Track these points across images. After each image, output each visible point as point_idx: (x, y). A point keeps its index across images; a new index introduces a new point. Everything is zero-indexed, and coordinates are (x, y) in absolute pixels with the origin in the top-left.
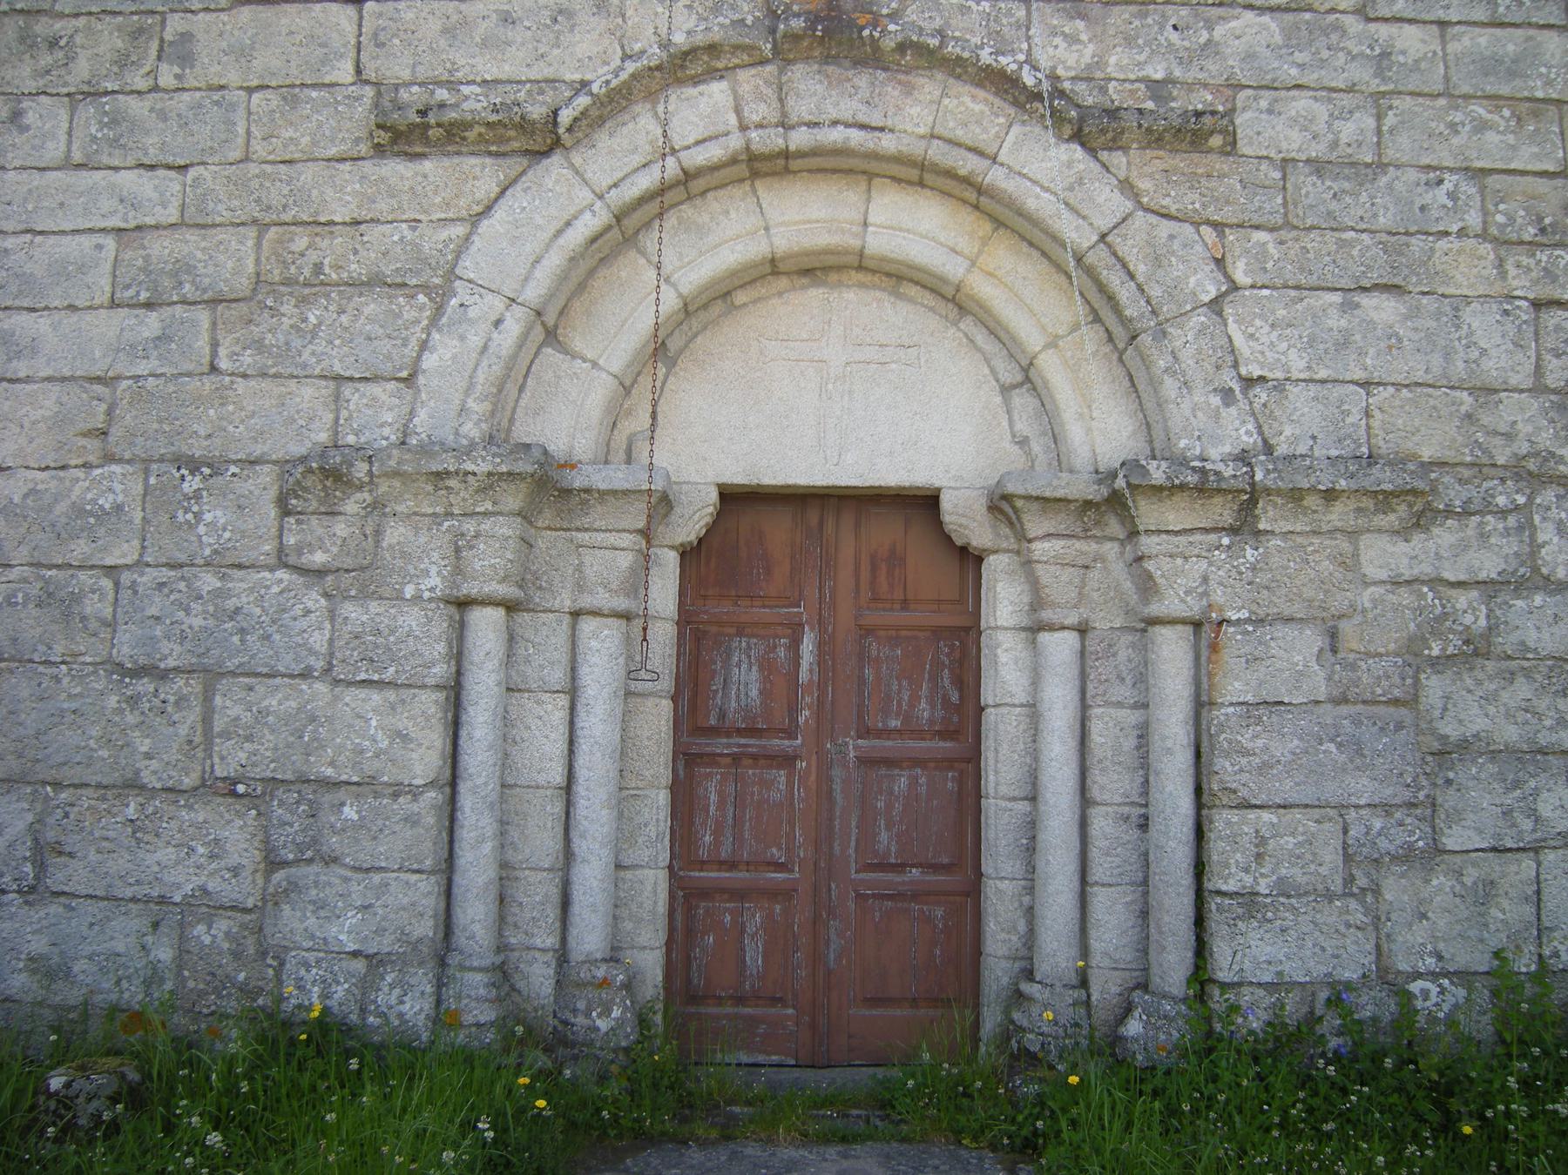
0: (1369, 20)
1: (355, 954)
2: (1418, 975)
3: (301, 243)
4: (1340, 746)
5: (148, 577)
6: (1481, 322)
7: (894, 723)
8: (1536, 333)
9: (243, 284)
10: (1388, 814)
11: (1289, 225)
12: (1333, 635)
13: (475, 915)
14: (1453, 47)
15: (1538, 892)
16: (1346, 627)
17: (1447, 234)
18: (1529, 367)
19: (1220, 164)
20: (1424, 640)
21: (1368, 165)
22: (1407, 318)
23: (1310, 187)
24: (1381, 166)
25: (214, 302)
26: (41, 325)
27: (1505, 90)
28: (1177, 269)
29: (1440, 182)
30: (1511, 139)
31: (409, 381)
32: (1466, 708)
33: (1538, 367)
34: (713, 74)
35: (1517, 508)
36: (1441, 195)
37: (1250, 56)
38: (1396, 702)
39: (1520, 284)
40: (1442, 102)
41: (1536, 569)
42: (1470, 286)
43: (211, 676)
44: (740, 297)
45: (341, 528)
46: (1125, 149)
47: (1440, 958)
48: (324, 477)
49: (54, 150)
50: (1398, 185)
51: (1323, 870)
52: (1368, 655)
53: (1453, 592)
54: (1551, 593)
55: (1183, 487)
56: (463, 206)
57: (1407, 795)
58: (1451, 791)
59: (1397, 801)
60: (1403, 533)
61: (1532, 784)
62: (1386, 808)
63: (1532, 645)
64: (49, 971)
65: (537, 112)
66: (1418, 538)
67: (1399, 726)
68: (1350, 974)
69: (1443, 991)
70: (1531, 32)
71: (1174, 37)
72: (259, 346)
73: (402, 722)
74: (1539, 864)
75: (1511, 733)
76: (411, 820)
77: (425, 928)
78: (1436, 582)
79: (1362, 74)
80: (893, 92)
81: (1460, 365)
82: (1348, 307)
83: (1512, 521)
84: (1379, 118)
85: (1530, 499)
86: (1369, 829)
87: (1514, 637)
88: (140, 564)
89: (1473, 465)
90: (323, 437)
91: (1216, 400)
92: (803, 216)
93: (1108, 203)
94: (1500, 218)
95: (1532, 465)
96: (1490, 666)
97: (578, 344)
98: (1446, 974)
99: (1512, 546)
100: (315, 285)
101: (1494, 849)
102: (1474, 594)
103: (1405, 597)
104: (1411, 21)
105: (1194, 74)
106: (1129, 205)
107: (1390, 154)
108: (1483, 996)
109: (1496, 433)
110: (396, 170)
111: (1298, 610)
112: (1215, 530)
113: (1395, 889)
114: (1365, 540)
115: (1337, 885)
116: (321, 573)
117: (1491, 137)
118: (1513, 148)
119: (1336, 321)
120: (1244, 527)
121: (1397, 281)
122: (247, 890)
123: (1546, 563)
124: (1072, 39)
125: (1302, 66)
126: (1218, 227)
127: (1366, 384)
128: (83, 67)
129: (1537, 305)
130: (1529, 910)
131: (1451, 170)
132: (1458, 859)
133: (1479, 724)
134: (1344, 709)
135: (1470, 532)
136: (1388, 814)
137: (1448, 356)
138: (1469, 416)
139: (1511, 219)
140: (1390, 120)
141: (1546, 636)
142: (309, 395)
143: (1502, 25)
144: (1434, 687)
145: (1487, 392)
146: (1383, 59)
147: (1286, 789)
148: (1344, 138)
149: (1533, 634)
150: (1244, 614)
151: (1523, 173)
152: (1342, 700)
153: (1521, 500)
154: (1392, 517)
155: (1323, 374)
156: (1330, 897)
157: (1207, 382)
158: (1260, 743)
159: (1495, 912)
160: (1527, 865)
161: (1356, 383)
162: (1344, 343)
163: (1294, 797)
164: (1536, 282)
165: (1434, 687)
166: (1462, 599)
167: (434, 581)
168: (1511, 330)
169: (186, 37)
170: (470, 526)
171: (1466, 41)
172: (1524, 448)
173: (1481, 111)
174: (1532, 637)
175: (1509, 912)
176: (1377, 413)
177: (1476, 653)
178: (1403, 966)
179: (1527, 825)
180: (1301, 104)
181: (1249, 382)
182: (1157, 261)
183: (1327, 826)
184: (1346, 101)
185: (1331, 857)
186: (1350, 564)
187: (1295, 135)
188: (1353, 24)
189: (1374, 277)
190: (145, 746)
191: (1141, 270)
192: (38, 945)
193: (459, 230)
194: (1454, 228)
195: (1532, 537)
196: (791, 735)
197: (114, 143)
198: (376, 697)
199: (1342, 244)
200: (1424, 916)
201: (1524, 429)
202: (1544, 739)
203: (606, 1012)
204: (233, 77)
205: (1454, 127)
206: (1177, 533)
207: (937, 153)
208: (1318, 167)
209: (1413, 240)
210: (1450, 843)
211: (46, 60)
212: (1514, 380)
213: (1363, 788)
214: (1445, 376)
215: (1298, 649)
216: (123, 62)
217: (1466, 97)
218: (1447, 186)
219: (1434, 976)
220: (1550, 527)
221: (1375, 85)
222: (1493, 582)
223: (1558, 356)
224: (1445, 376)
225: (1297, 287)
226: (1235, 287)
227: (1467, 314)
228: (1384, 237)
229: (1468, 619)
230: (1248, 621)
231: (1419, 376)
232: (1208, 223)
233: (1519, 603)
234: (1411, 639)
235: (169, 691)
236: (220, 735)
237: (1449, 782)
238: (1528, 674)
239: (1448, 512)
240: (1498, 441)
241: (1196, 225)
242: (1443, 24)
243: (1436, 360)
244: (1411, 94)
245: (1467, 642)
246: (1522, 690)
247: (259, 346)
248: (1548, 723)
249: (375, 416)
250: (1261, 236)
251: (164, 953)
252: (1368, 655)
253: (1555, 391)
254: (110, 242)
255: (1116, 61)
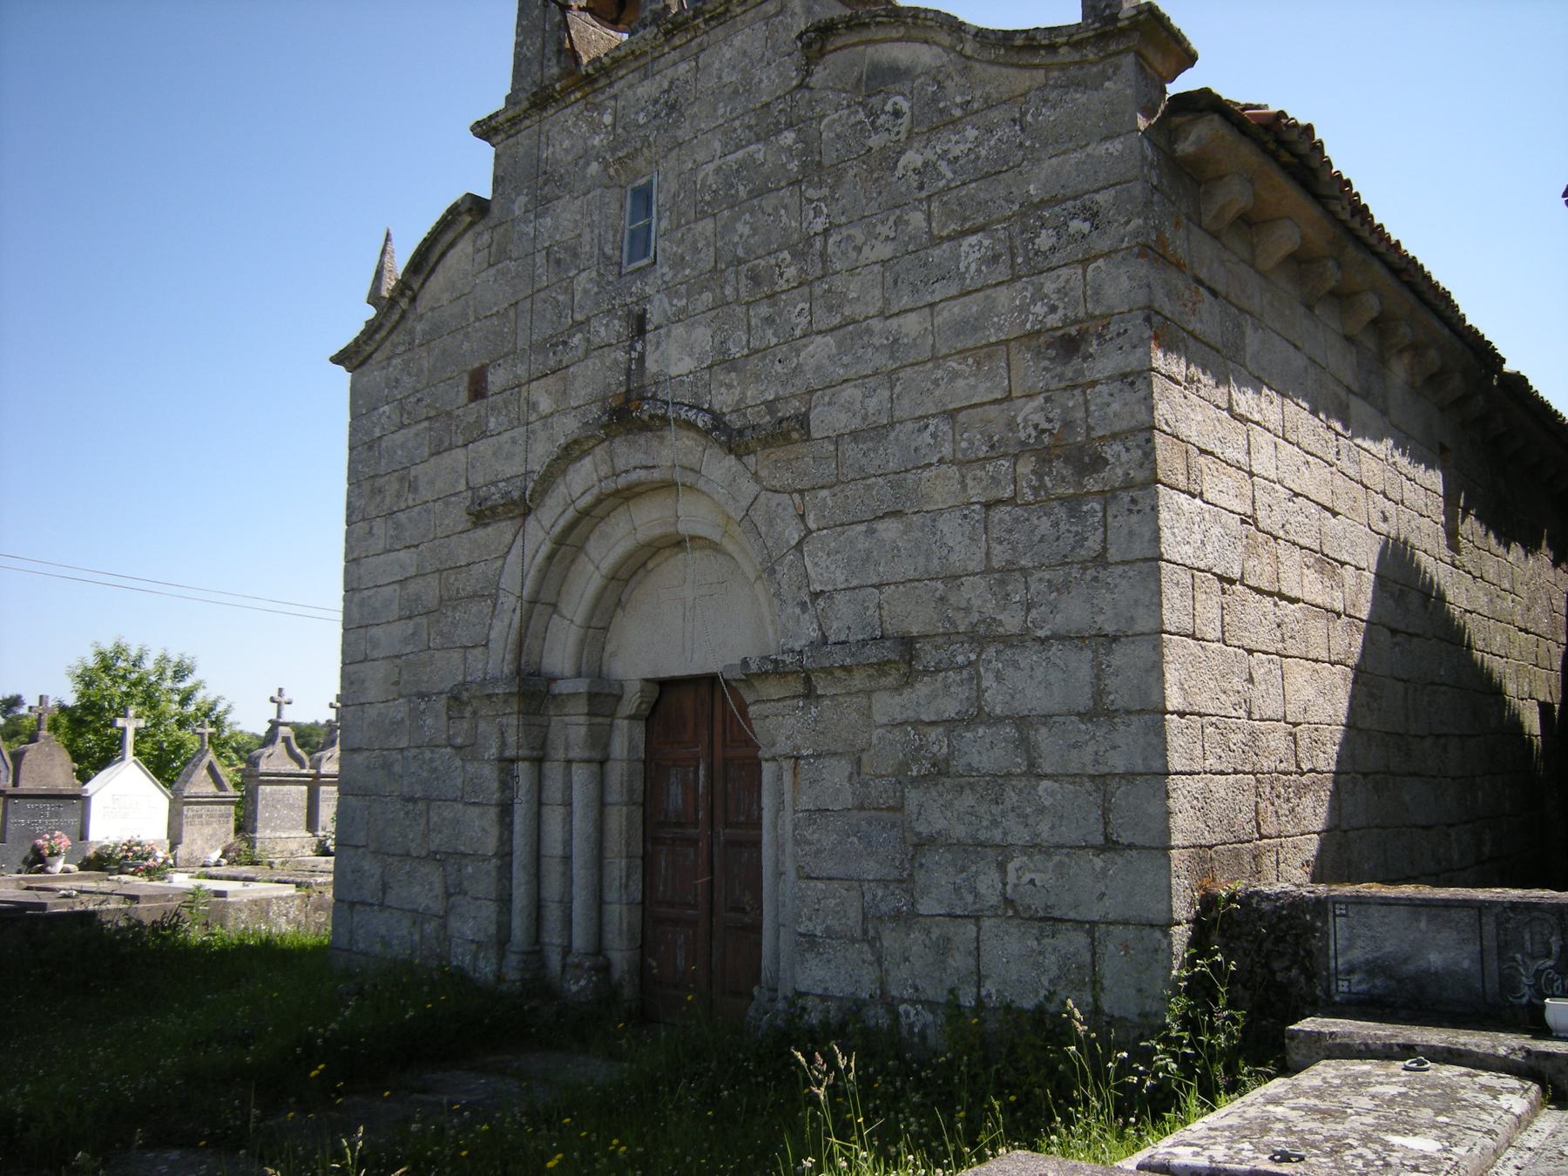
0: (887, 318)
1: (472, 941)
2: (904, 1001)
4: (860, 839)
6: (949, 527)
7: (742, 819)
8: (986, 528)
10: (887, 887)
11: (839, 482)
12: (859, 762)
13: (519, 924)
14: (938, 321)
15: (978, 948)
17: (931, 465)
18: (981, 554)
19: (802, 449)
20: (908, 765)
21: (884, 426)
22: (905, 533)
23: (850, 450)
24: (892, 425)
27: (970, 344)
29: (927, 426)
30: (972, 381)
31: (486, 645)
32: (936, 813)
33: (988, 554)
34: (585, 453)
35: (970, 663)
36: (926, 437)
37: (819, 367)
38: (889, 809)
39: (976, 493)
40: (930, 365)
41: (980, 709)
42: (944, 502)
44: (650, 565)
46: (754, 452)
47: (917, 989)
50: (902, 437)
51: (850, 923)
52: (877, 776)
53: (928, 729)
54: (989, 726)
55: (767, 672)
57: (896, 873)
58: (922, 872)
59: (891, 877)
60: (897, 689)
61: (974, 868)
62: (883, 882)
63: (975, 765)
65: (516, 495)
66: (906, 692)
67: (894, 825)
68: (865, 995)
69: (917, 1014)
70: (988, 292)
71: (778, 367)
74: (979, 929)
76: (488, 873)
77: (973, 969)
78: (917, 723)
79: (882, 361)
80: (655, 443)
81: (936, 561)
83: (965, 673)
84: (892, 388)
85: (979, 655)
86: (875, 896)
87: (964, 761)
89: (944, 634)
90: (460, 678)
91: (798, 610)
92: (647, 519)
94: (964, 445)
95: (982, 629)
96: (947, 781)
97: (564, 612)
98: (921, 1002)
99: (964, 692)
101: (949, 915)
102: (941, 729)
103: (897, 735)
104: (912, 310)
105: (790, 390)
106: (758, 488)
107: (898, 414)
108: (941, 1019)
109: (959, 609)
112: (794, 697)
113: (890, 939)
114: (876, 696)
115: (858, 933)
117: (961, 383)
118: (974, 387)
119: (863, 544)
121: (899, 507)
122: (437, 907)
123: (987, 704)
124: (730, 386)
125: (845, 366)
126: (801, 492)
127: (877, 586)
129: (988, 506)
130: (971, 961)
131: (933, 416)
132: (928, 921)
133: (940, 824)
134: (863, 814)
135: (938, 685)
136: (887, 887)
137: (928, 558)
138: (942, 599)
139: (971, 443)
140: (898, 389)
141: (985, 758)
143: (969, 293)
144: (913, 797)
145: (953, 579)
147: (830, 867)
148: (871, 411)
149: (976, 758)
150: (810, 751)
151: (982, 404)
152: (861, 808)
153: (973, 657)
154: (890, 679)
155: (854, 583)
156: (853, 941)
157: (794, 599)
158: (816, 836)
159: (950, 961)
161: (873, 586)
162: (867, 558)
163: (833, 873)
164: (984, 489)
165: (913, 797)
166: (934, 734)
167: (494, 750)
168: (967, 528)
170: (505, 721)
171: (946, 314)
172: (975, 617)
173: (954, 365)
174: (975, 760)
175: (959, 961)
176: (886, 606)
177: (940, 773)
178: (895, 993)
179: (970, 898)
180: (850, 393)
183: (853, 893)
184: (872, 382)
185: (854, 914)
186: (867, 713)
187: (843, 417)
188: (876, 324)
189: (885, 508)
191: (763, 529)
192: (383, 931)
193: (500, 563)
194: (935, 459)
195: (978, 684)
196: (696, 824)
199: (868, 488)
200: (907, 959)
201: (976, 603)
202: (983, 835)
203: (577, 982)
205: (936, 382)
206: (779, 700)
207: (557, 529)
208: (855, 435)
209: (909, 476)
210: (922, 909)
212: (971, 566)
214: (927, 571)
215: (836, 773)
217: (945, 357)
218: (931, 428)
219: (913, 1002)
220: (991, 675)
221: (891, 365)
222: (953, 720)
223: (1001, 543)
224: (927, 571)
225: (842, 525)
226: (810, 532)
227: (940, 525)
228: (891, 477)
229: (935, 749)
230: (812, 756)
231: (911, 575)
232: (796, 491)
233: (969, 735)
234: (901, 764)
237: (921, 865)
238: (972, 786)
239: (926, 672)
240: (962, 614)
241: (790, 494)
242: (932, 305)
243: (921, 561)
244: (912, 365)
245: (934, 765)
246: (969, 799)
248: (985, 823)
250: (825, 493)
251: (417, 937)
252: (877, 776)
253: (998, 571)
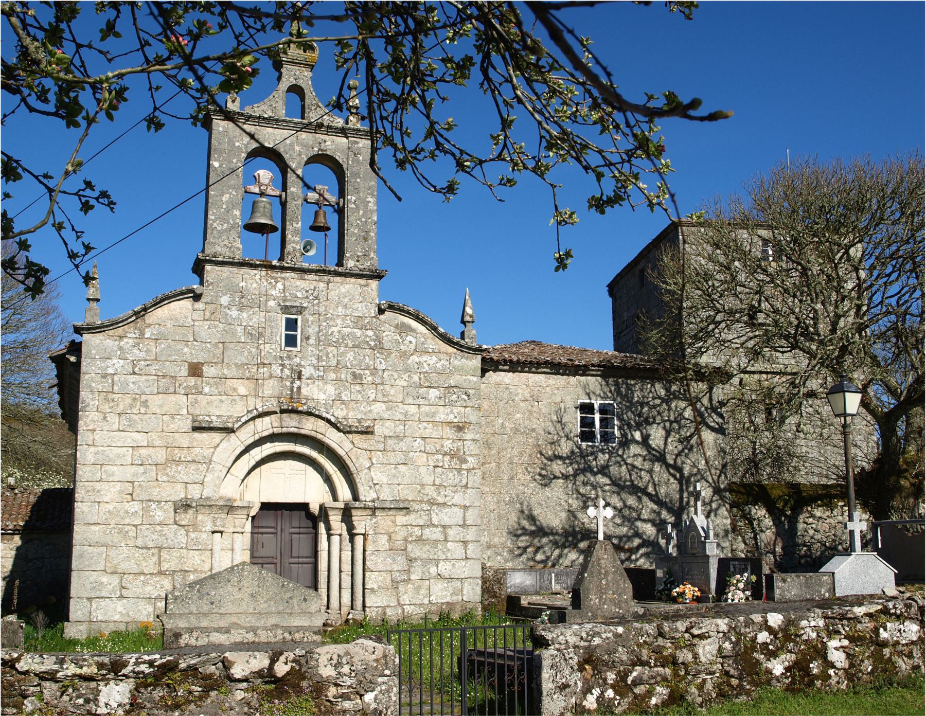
3: (176, 452)
5: (143, 528)
6: (423, 470)
9: (163, 461)
16: (393, 535)
25: (156, 465)
26: (115, 468)
28: (361, 460)
43: (160, 549)
45: (188, 516)
48: (184, 506)
49: (115, 427)
56: (213, 445)
64: (588, 589)
72: (168, 475)
73: (203, 558)
75: (425, 556)
79: (402, 417)
82: (395, 468)
88: (142, 524)
90: (183, 496)
93: (348, 446)
100: (178, 462)
110: (197, 435)
111: (383, 532)
116: (184, 526)
120: (374, 514)
124: (342, 409)
128: (121, 407)
133: (419, 554)
142: (180, 487)
144: (410, 547)
146: (406, 414)
160: (427, 582)
166: (416, 529)
169: (147, 401)
180: (388, 423)
181: (375, 484)
182: (357, 459)
184: (398, 422)
186: (394, 522)
188: (400, 405)
190: (145, 564)
197: (130, 426)
198: (197, 552)
204: (158, 411)
211: (112, 404)
213: (395, 567)
216: (131, 407)
226: (373, 464)
235: (150, 552)
236: (347, 123)
246: (428, 547)
247: (168, 475)
249: (195, 493)
250: (379, 453)
254: (130, 449)
255: (351, 414)
